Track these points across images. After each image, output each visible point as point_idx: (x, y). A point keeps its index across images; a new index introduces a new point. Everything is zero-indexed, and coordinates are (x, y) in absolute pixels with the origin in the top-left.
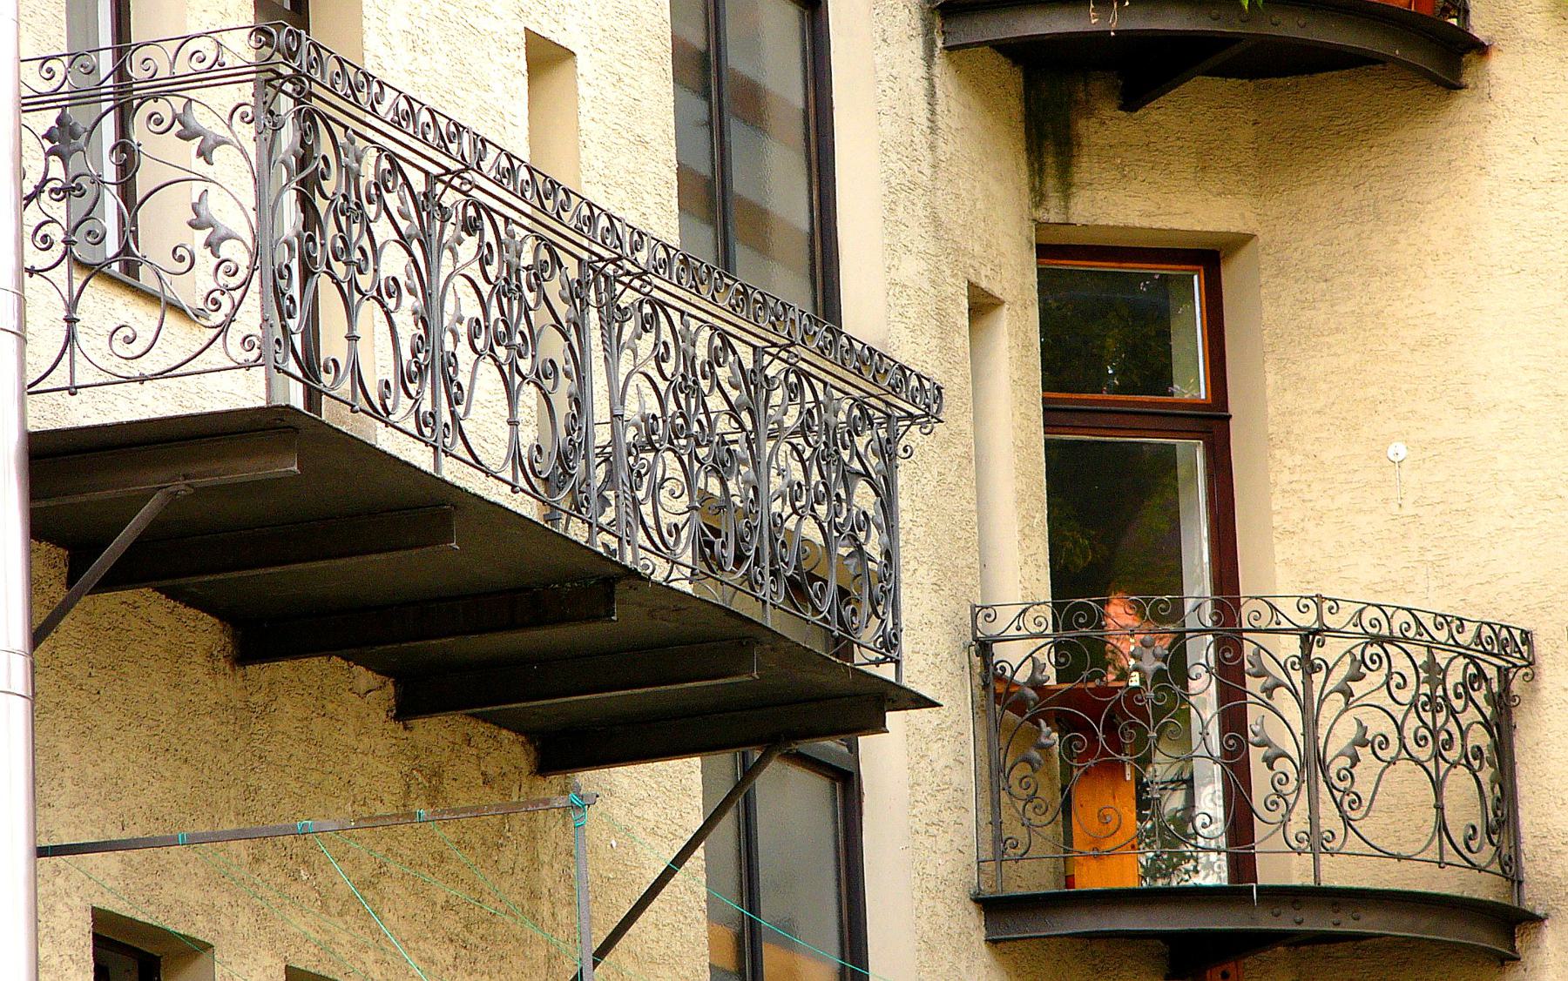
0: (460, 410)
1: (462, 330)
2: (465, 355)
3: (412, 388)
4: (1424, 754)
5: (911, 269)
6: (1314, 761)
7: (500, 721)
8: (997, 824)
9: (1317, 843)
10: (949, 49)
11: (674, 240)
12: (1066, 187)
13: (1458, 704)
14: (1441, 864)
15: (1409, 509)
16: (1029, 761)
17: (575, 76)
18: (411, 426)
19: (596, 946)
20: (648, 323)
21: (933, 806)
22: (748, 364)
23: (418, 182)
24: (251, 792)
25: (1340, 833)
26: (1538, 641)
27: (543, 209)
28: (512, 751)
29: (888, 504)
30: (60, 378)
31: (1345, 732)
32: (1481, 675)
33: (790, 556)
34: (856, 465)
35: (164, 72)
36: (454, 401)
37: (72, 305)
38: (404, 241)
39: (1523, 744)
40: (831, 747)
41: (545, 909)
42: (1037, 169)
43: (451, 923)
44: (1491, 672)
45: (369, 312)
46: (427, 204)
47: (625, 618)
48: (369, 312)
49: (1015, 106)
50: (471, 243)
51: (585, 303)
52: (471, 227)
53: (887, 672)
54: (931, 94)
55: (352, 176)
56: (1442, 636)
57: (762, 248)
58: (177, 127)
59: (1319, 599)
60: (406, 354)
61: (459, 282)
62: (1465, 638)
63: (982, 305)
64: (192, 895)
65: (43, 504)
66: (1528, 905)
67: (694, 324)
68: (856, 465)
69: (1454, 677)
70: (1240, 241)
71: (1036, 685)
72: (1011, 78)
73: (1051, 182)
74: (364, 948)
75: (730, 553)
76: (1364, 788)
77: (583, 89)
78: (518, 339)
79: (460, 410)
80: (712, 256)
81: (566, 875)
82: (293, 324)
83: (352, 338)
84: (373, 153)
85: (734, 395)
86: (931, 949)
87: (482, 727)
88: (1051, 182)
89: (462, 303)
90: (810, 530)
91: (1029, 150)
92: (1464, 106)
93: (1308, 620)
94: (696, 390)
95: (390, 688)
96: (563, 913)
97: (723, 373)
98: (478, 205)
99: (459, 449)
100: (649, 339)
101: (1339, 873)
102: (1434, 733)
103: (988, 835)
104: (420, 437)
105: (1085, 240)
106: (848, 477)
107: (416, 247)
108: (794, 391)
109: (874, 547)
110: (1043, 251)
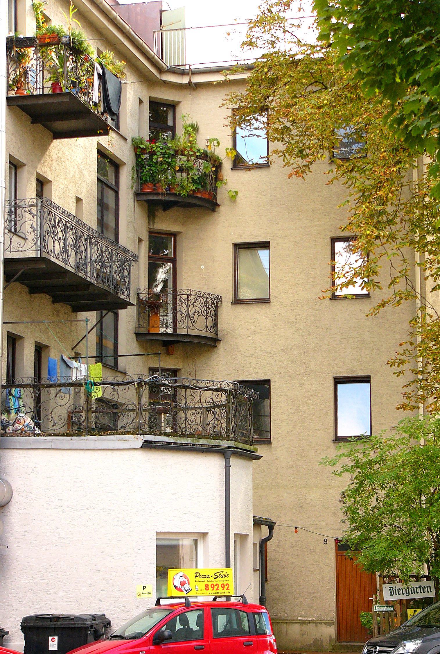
0: (69, 258)
1: (70, 245)
2: (70, 250)
3: (62, 254)
4: (205, 314)
5: (130, 235)
6: (188, 315)
7: (67, 304)
8: (139, 322)
9: (188, 328)
10: (137, 200)
11: (96, 230)
12: (154, 223)
13: (210, 307)
14: (206, 332)
15: (204, 276)
16: (144, 313)
17: (82, 203)
18: (62, 260)
19: (86, 338)
20: (96, 245)
21: (129, 319)
22: (110, 252)
23: (64, 223)
24: (31, 314)
25: (191, 326)
26: (222, 298)
27: (82, 227)
28: (69, 309)
29: (129, 274)
30: (9, 250)
31: (193, 311)
32: (214, 303)
33: (115, 282)
34: (125, 268)
35: (27, 204)
36: (68, 256)
37: (11, 239)
38: (62, 231)
39: (219, 314)
40: (115, 311)
41: (72, 333)
42: (149, 220)
43: (59, 335)
44: (215, 302)
45: (57, 242)
46: (65, 226)
47: (91, 290)
48: (57, 242)
49: (146, 210)
50: (71, 232)
51: (87, 242)
52: (72, 229)
53: (128, 300)
54: (134, 207)
55: (55, 221)
56: (208, 297)
57: (107, 230)
58: (29, 212)
59: (190, 290)
60: (62, 249)
61: (70, 238)
62: (212, 297)
63: (140, 240)
64: (22, 329)
65: (7, 269)
66: (219, 338)
67: (103, 245)
68: (125, 268)
69: (210, 303)
70: (179, 233)
71: (146, 300)
72: (146, 205)
73: (151, 222)
74: (46, 338)
75: (106, 281)
76: (195, 319)
77: (84, 205)
78: (77, 247)
79: (69, 258)
80: (114, 239)
81: (76, 328)
82: (45, 244)
83: (54, 246)
84: (58, 218)
85: (108, 256)
86: (128, 341)
87: (65, 305)
88: (151, 222)
89: (70, 241)
90: (118, 278)
91: (148, 217)
92: (216, 214)
93: (188, 293)
94: (103, 256)
95: (52, 298)
96: (75, 334)
97: (107, 253)
98: (73, 226)
99: (69, 264)
100: (96, 247)
101: (191, 332)
102: (206, 312)
103: (137, 323)
104: (63, 262)
105: (157, 231)
106: (124, 269)
107: (64, 232)
108: (117, 256)
109: (127, 281)
110: (150, 232)
